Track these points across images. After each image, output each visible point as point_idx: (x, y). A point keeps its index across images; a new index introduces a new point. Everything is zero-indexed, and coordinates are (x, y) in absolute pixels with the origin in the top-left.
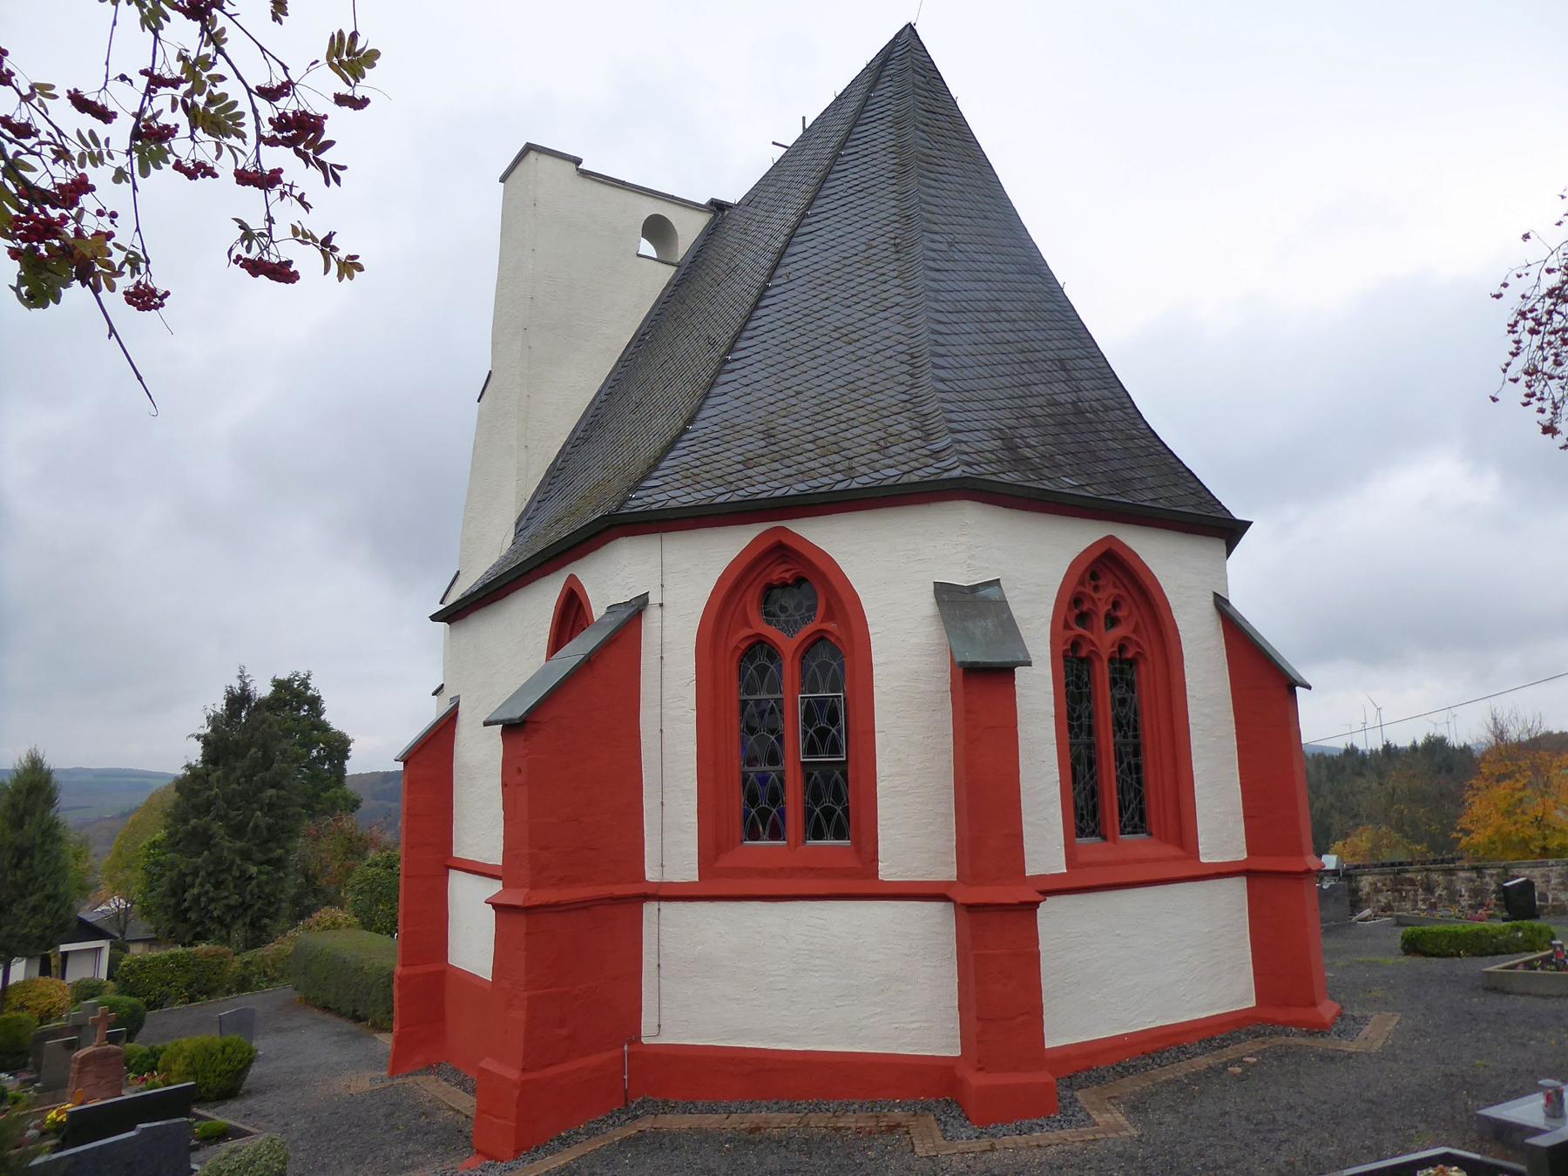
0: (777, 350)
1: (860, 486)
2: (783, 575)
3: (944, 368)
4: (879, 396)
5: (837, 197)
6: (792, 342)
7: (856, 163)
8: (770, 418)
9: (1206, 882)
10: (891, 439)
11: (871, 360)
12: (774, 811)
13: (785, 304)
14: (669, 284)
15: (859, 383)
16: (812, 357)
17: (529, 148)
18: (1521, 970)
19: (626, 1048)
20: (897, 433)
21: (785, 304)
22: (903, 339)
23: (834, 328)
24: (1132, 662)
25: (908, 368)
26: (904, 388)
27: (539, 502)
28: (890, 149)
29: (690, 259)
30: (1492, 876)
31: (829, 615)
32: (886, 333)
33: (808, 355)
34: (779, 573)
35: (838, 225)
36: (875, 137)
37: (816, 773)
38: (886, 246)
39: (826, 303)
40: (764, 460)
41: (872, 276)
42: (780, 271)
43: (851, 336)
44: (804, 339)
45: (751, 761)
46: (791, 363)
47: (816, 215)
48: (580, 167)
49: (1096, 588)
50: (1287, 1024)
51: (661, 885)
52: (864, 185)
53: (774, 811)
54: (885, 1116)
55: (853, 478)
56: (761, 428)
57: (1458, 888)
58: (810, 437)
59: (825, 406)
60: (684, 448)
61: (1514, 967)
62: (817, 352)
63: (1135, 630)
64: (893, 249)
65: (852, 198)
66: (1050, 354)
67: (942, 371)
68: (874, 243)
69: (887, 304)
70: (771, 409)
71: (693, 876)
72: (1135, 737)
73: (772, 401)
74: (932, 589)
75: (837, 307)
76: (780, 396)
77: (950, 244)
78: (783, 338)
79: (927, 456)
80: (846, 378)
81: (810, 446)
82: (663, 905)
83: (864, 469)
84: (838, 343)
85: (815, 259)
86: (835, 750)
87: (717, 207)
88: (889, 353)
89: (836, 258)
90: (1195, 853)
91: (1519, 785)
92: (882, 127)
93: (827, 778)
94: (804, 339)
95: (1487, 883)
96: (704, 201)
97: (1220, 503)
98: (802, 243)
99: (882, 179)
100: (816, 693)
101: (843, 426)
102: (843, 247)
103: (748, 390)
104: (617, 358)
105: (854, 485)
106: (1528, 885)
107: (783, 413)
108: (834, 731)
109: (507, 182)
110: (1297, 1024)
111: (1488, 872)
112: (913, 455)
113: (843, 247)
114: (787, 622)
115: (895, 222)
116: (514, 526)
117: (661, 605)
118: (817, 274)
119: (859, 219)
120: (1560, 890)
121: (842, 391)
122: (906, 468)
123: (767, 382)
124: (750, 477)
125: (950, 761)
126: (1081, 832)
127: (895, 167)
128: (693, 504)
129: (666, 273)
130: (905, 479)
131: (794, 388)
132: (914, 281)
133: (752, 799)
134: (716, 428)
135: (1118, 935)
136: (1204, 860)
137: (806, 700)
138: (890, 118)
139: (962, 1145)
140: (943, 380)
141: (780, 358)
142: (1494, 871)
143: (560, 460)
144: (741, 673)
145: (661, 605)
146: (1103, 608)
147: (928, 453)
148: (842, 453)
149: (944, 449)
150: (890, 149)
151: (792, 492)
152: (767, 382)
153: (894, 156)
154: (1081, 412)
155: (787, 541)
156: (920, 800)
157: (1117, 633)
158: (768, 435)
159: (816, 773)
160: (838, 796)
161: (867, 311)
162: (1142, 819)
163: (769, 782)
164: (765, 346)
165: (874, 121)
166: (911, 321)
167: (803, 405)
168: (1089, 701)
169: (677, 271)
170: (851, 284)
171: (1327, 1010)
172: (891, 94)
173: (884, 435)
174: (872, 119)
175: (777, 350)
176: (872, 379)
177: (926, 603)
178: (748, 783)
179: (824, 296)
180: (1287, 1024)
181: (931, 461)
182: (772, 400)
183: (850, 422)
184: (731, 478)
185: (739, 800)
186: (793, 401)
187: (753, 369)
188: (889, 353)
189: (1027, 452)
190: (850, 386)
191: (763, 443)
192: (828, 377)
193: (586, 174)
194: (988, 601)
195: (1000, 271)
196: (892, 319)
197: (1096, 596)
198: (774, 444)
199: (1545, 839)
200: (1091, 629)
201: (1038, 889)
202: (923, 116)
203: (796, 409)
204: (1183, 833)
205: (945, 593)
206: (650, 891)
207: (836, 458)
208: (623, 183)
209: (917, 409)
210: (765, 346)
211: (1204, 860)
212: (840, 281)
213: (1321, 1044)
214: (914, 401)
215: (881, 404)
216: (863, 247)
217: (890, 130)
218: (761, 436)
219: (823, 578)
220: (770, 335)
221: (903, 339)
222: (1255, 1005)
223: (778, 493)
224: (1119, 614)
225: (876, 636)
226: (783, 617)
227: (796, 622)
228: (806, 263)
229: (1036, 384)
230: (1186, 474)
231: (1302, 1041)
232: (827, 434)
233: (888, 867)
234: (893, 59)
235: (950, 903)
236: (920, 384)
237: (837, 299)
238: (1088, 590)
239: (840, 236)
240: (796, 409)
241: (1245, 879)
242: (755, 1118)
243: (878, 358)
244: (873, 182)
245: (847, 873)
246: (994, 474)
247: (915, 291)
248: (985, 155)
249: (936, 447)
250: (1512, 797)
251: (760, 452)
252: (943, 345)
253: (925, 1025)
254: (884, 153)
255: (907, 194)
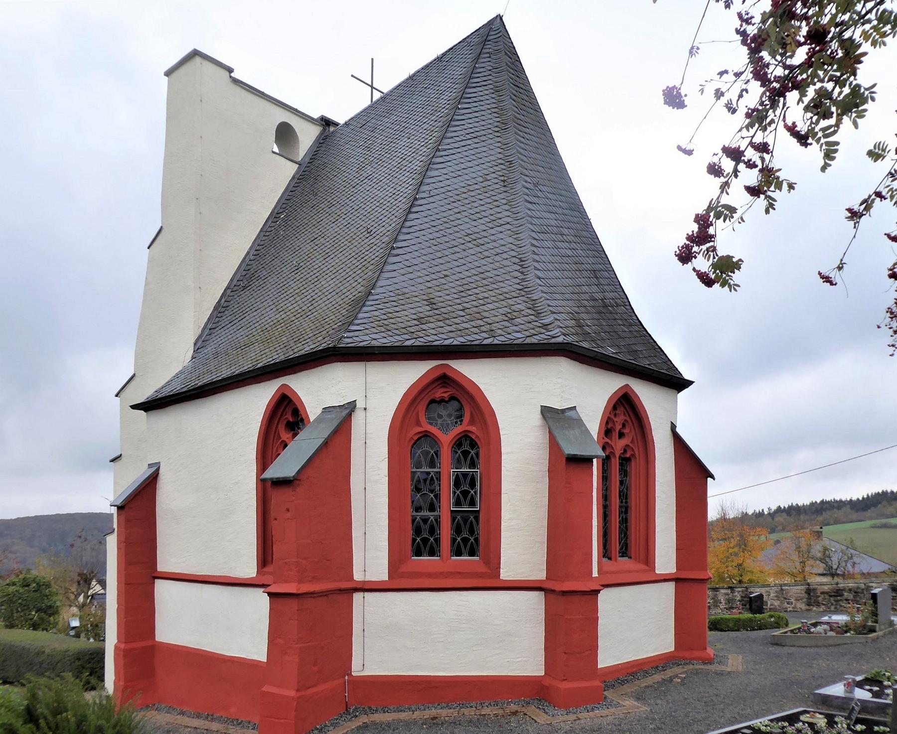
0: (428, 244)
1: (500, 343)
2: (442, 395)
3: (539, 270)
4: (502, 284)
5: (458, 139)
6: (438, 240)
7: (470, 116)
8: (429, 291)
9: (656, 584)
10: (515, 314)
11: (493, 259)
12: (432, 539)
13: (430, 213)
14: (293, 177)
15: (487, 274)
16: (453, 252)
17: (195, 54)
18: (789, 634)
19: (346, 678)
20: (518, 310)
21: (430, 213)
22: (514, 247)
23: (466, 234)
24: (628, 460)
25: (519, 268)
26: (518, 281)
27: (210, 329)
28: (494, 110)
29: (307, 160)
30: (739, 592)
31: (472, 422)
32: (502, 242)
33: (450, 250)
34: (440, 393)
35: (462, 160)
36: (482, 98)
37: (459, 517)
38: (496, 181)
39: (459, 216)
40: (431, 319)
41: (489, 200)
42: (423, 188)
43: (479, 241)
44: (446, 239)
45: (418, 509)
46: (439, 255)
47: (445, 150)
48: (232, 75)
49: (615, 415)
50: (691, 659)
51: (364, 582)
52: (478, 134)
53: (432, 539)
54: (506, 708)
55: (495, 337)
56: (425, 297)
57: (719, 598)
58: (460, 307)
59: (467, 287)
60: (372, 305)
61: (786, 632)
62: (456, 249)
63: (632, 442)
64: (502, 183)
65: (469, 142)
66: (588, 266)
67: (538, 272)
68: (488, 177)
69: (501, 222)
70: (429, 285)
71: (385, 577)
72: (626, 502)
73: (429, 280)
74: (540, 410)
75: (467, 220)
76: (433, 276)
77: (536, 185)
78: (431, 237)
79: (540, 327)
80: (479, 269)
81: (462, 313)
82: (367, 594)
83: (500, 332)
84: (470, 245)
85: (448, 182)
86: (472, 503)
87: (326, 122)
88: (505, 256)
89: (463, 184)
90: (653, 569)
91: (732, 545)
92: (487, 92)
93: (465, 521)
94: (446, 239)
95: (736, 596)
96: (316, 116)
97: (677, 369)
98: (437, 169)
99: (490, 131)
100: (461, 469)
101: (481, 302)
102: (467, 177)
103: (410, 270)
104: (260, 229)
105: (496, 342)
106: (761, 596)
107: (438, 288)
108: (472, 492)
109: (170, 76)
110: (697, 659)
111: (736, 590)
112: (530, 326)
113: (467, 177)
114: (442, 425)
115: (502, 164)
116: (193, 345)
117: (365, 409)
118: (450, 194)
119: (475, 158)
120: (774, 600)
121: (476, 278)
122: (527, 333)
123: (423, 266)
124: (424, 330)
125: (545, 512)
126: (604, 556)
127: (498, 124)
128: (388, 345)
129: (289, 170)
130: (528, 341)
131: (442, 272)
132: (518, 208)
133: (418, 531)
134: (391, 294)
135: (619, 611)
136: (657, 572)
137: (456, 473)
138: (491, 86)
139: (561, 718)
140: (539, 278)
141: (430, 250)
142: (740, 589)
143: (223, 300)
144: (412, 454)
145: (365, 409)
146: (618, 427)
147: (540, 325)
148: (484, 320)
149: (550, 324)
150: (494, 110)
151: (455, 343)
152: (423, 266)
153: (497, 116)
154: (606, 306)
155: (449, 374)
156: (527, 533)
157: (622, 443)
158: (431, 303)
159: (459, 517)
160: (472, 531)
161: (487, 225)
162: (626, 549)
163: (429, 522)
164: (419, 240)
165: (480, 86)
166: (518, 236)
167: (451, 284)
168: (606, 481)
169: (299, 168)
170: (475, 205)
171: (710, 651)
172: (491, 68)
173: (510, 311)
174: (478, 85)
175: (428, 244)
176: (496, 272)
177: (536, 418)
178: (416, 522)
179: (457, 210)
180: (691, 659)
181: (544, 331)
182: (428, 279)
183: (486, 300)
184: (412, 330)
185: (410, 533)
186: (443, 281)
187: (412, 255)
188: (505, 256)
189: (587, 329)
190: (482, 276)
191: (428, 308)
192: (465, 268)
193: (236, 81)
194: (570, 418)
195: (560, 207)
196: (505, 233)
197: (615, 420)
198: (436, 309)
199: (741, 576)
200: (611, 439)
201: (601, 584)
202: (513, 89)
203: (446, 287)
204: (648, 559)
205: (546, 412)
206: (359, 586)
207: (480, 323)
208: (263, 93)
209: (529, 296)
210: (419, 240)
211: (657, 572)
212: (467, 201)
213: (712, 668)
214: (526, 290)
215: (504, 290)
216: (481, 179)
217: (493, 96)
218: (425, 303)
219: (471, 398)
220: (422, 232)
221: (514, 247)
222: (673, 650)
223: (447, 342)
224: (626, 431)
225: (504, 436)
226: (439, 421)
227: (448, 424)
228: (441, 184)
229: (583, 285)
230: (659, 350)
231: (702, 667)
232: (471, 306)
233: (506, 572)
234: (490, 41)
235: (542, 592)
236: (528, 279)
237: (466, 214)
238: (612, 416)
239: (464, 169)
240: (446, 287)
241: (674, 583)
242: (433, 712)
243: (497, 258)
244: (483, 133)
245: (481, 575)
246: (577, 342)
247: (520, 215)
248: (546, 123)
249: (545, 321)
250: (728, 551)
251: (427, 313)
252: (538, 255)
253: (525, 659)
254: (489, 112)
255: (508, 145)
